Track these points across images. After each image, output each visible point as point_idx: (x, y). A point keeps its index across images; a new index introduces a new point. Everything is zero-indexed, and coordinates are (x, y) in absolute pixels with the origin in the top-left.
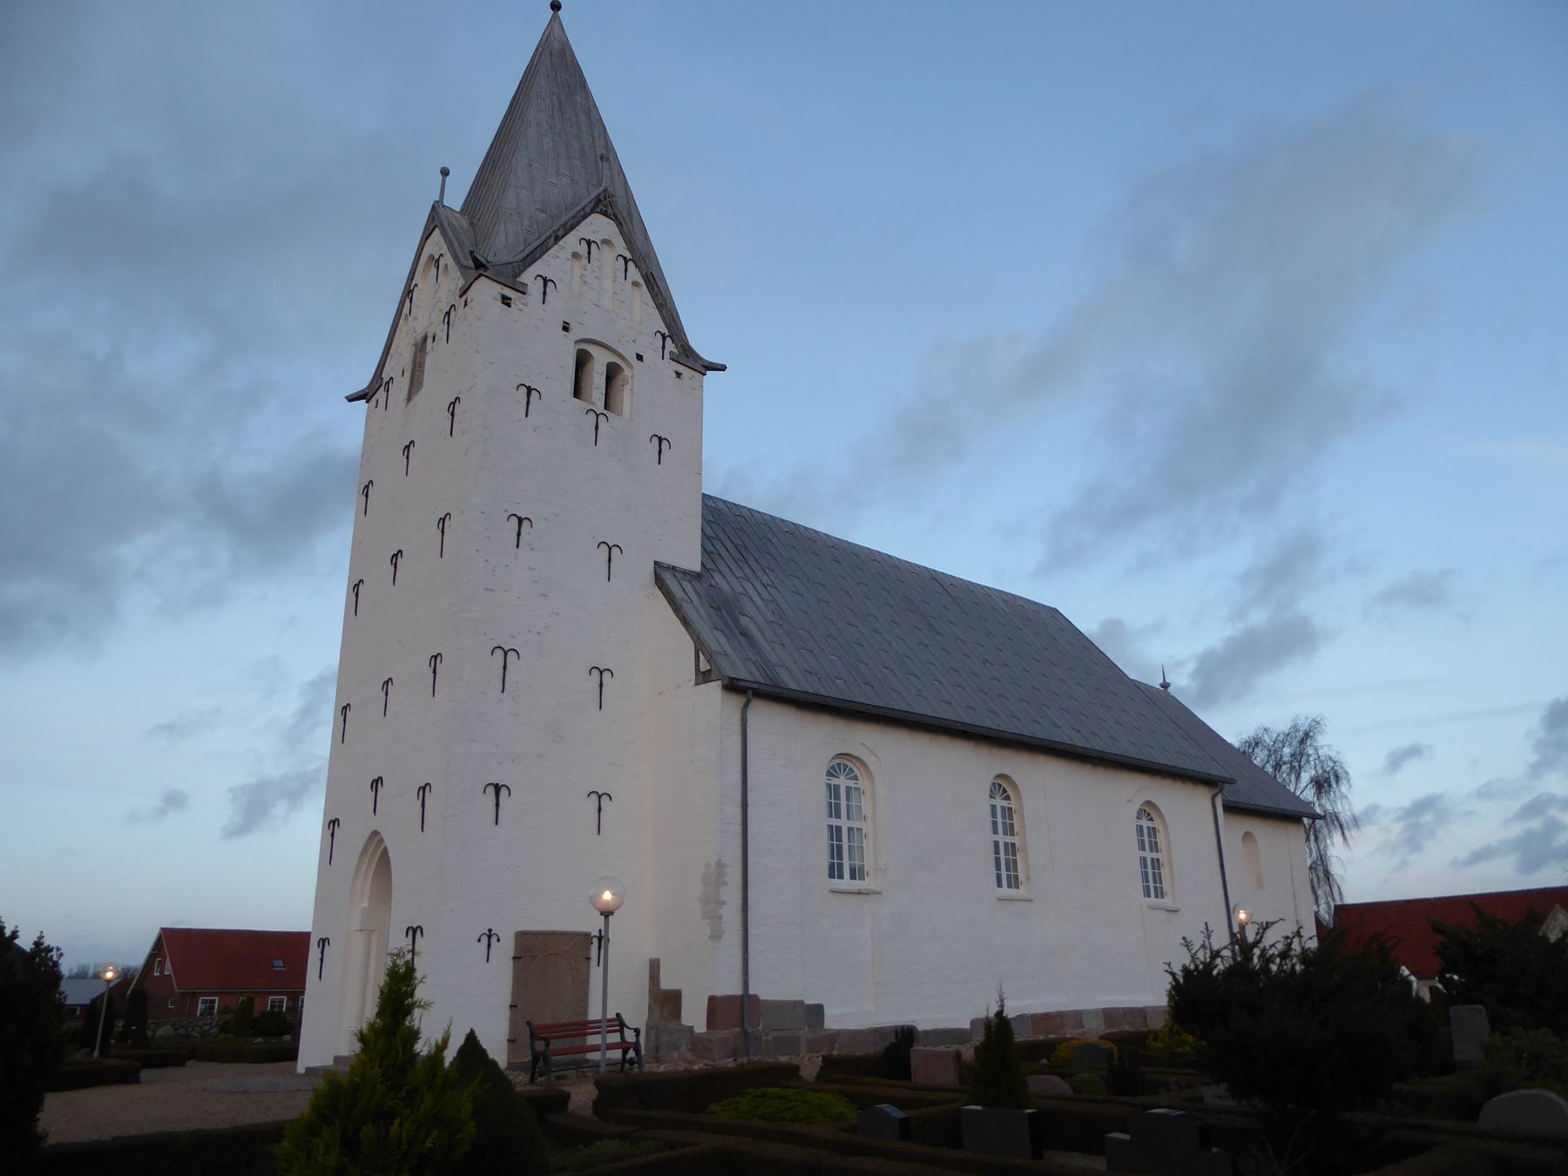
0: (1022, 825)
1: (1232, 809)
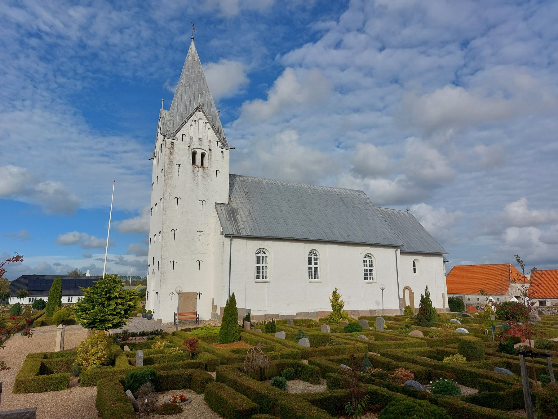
0: (320, 263)
1: (402, 253)
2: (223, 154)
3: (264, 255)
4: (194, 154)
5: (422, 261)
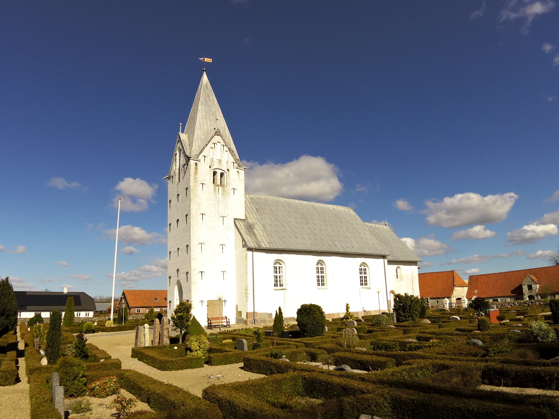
1: (390, 262)
2: (239, 174)
3: (280, 266)
4: (215, 173)
5: (404, 269)
